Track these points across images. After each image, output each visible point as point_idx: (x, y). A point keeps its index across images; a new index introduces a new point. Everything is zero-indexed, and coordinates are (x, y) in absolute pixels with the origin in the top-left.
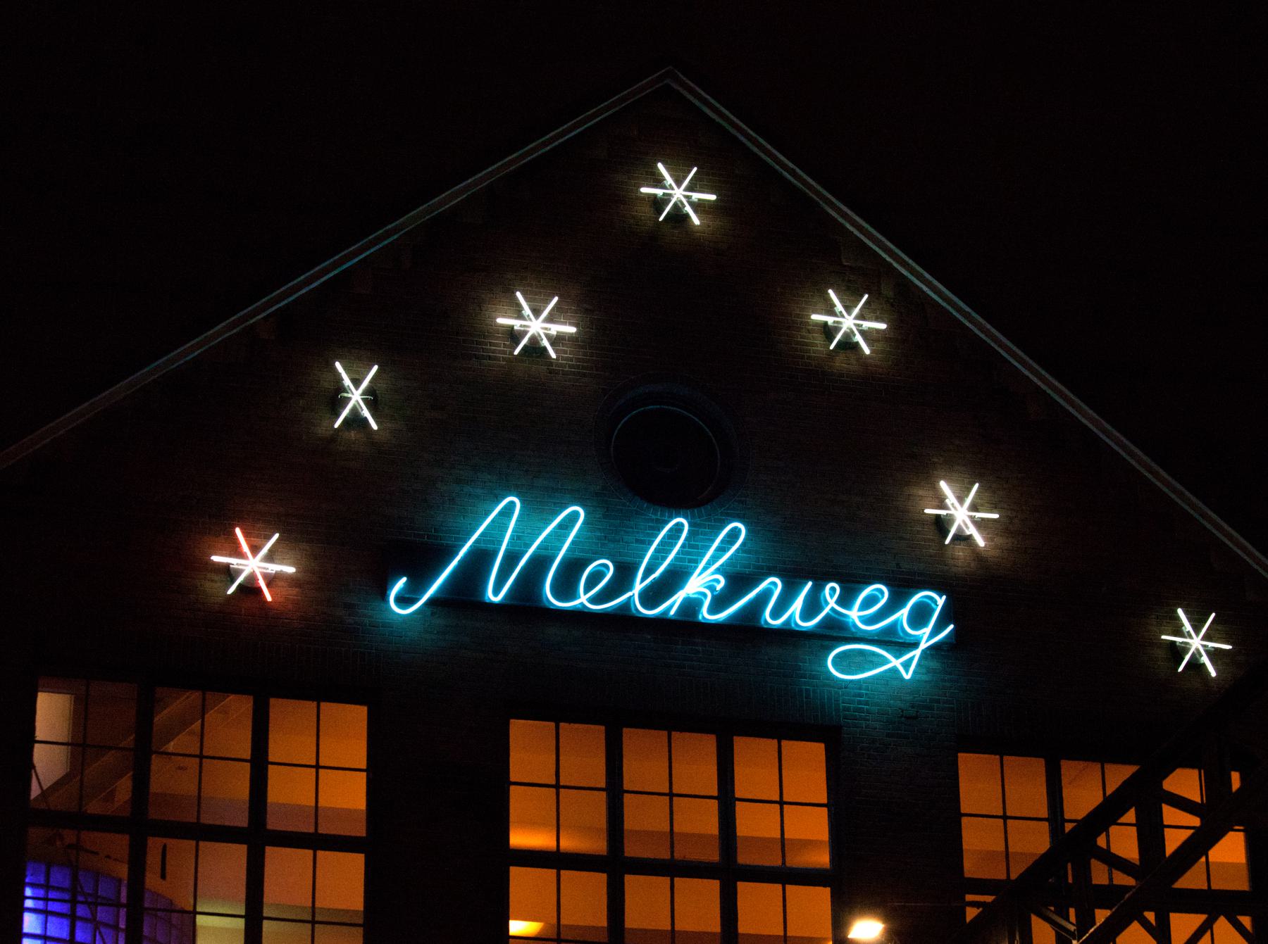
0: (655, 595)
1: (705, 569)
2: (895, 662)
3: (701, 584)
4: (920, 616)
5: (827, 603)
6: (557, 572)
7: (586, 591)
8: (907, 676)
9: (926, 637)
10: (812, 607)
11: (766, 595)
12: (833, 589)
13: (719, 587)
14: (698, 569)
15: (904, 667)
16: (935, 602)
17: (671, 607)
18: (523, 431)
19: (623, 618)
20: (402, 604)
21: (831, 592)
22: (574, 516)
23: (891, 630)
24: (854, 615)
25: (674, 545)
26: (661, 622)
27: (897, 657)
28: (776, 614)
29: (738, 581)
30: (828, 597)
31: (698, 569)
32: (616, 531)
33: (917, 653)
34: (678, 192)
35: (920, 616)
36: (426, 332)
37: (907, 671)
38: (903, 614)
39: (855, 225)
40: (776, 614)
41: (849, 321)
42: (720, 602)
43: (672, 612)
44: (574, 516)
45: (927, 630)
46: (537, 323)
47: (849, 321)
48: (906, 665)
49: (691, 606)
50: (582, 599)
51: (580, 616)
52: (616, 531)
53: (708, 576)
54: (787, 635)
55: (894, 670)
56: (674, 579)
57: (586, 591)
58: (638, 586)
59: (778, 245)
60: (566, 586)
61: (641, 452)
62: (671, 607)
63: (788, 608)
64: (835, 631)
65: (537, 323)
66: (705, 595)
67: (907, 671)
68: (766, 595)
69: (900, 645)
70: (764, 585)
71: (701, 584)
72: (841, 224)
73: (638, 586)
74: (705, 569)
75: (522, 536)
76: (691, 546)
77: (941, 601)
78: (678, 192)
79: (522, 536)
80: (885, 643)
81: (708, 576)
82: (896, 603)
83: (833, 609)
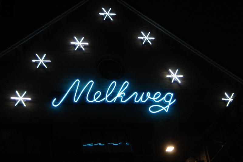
0: (110, 98)
1: (121, 92)
2: (164, 108)
3: (120, 94)
4: (168, 98)
5: (147, 97)
6: (88, 96)
7: (95, 98)
8: (167, 111)
9: (170, 103)
10: (144, 98)
11: (135, 96)
12: (149, 94)
13: (124, 95)
14: (119, 92)
15: (166, 109)
16: (171, 95)
17: (114, 100)
18: (81, 66)
19: (104, 103)
20: (55, 104)
21: (148, 94)
22: (91, 83)
23: (163, 101)
24: (154, 99)
25: (113, 88)
26: (113, 103)
27: (164, 107)
28: (137, 100)
29: (128, 93)
30: (148, 96)
31: (119, 92)
32: (101, 86)
33: (168, 106)
34: (107, 14)
35: (168, 98)
36: (57, 48)
37: (167, 110)
38: (164, 98)
39: (146, 18)
40: (137, 100)
41: (146, 38)
42: (125, 98)
43: (115, 101)
44: (91, 83)
45: (170, 101)
46: (79, 43)
47: (146, 38)
48: (166, 109)
49: (119, 99)
50: (95, 100)
51: (95, 104)
52: (101, 86)
53: (122, 93)
54: (140, 104)
55: (164, 110)
56: (114, 94)
57: (95, 98)
58: (107, 96)
59: (128, 23)
60: (91, 98)
61: (102, 68)
62: (114, 100)
63: (139, 99)
64: (150, 102)
65: (79, 43)
66: (121, 97)
67: (167, 110)
68: (135, 96)
69: (164, 104)
70: (134, 94)
71: (120, 94)
72: (87, 146)
73: (107, 96)
74: (121, 92)
75: (79, 89)
76: (117, 88)
77: (172, 95)
78: (107, 14)
79: (79, 89)
80: (161, 103)
81: (122, 93)
82: (162, 96)
83: (149, 98)
